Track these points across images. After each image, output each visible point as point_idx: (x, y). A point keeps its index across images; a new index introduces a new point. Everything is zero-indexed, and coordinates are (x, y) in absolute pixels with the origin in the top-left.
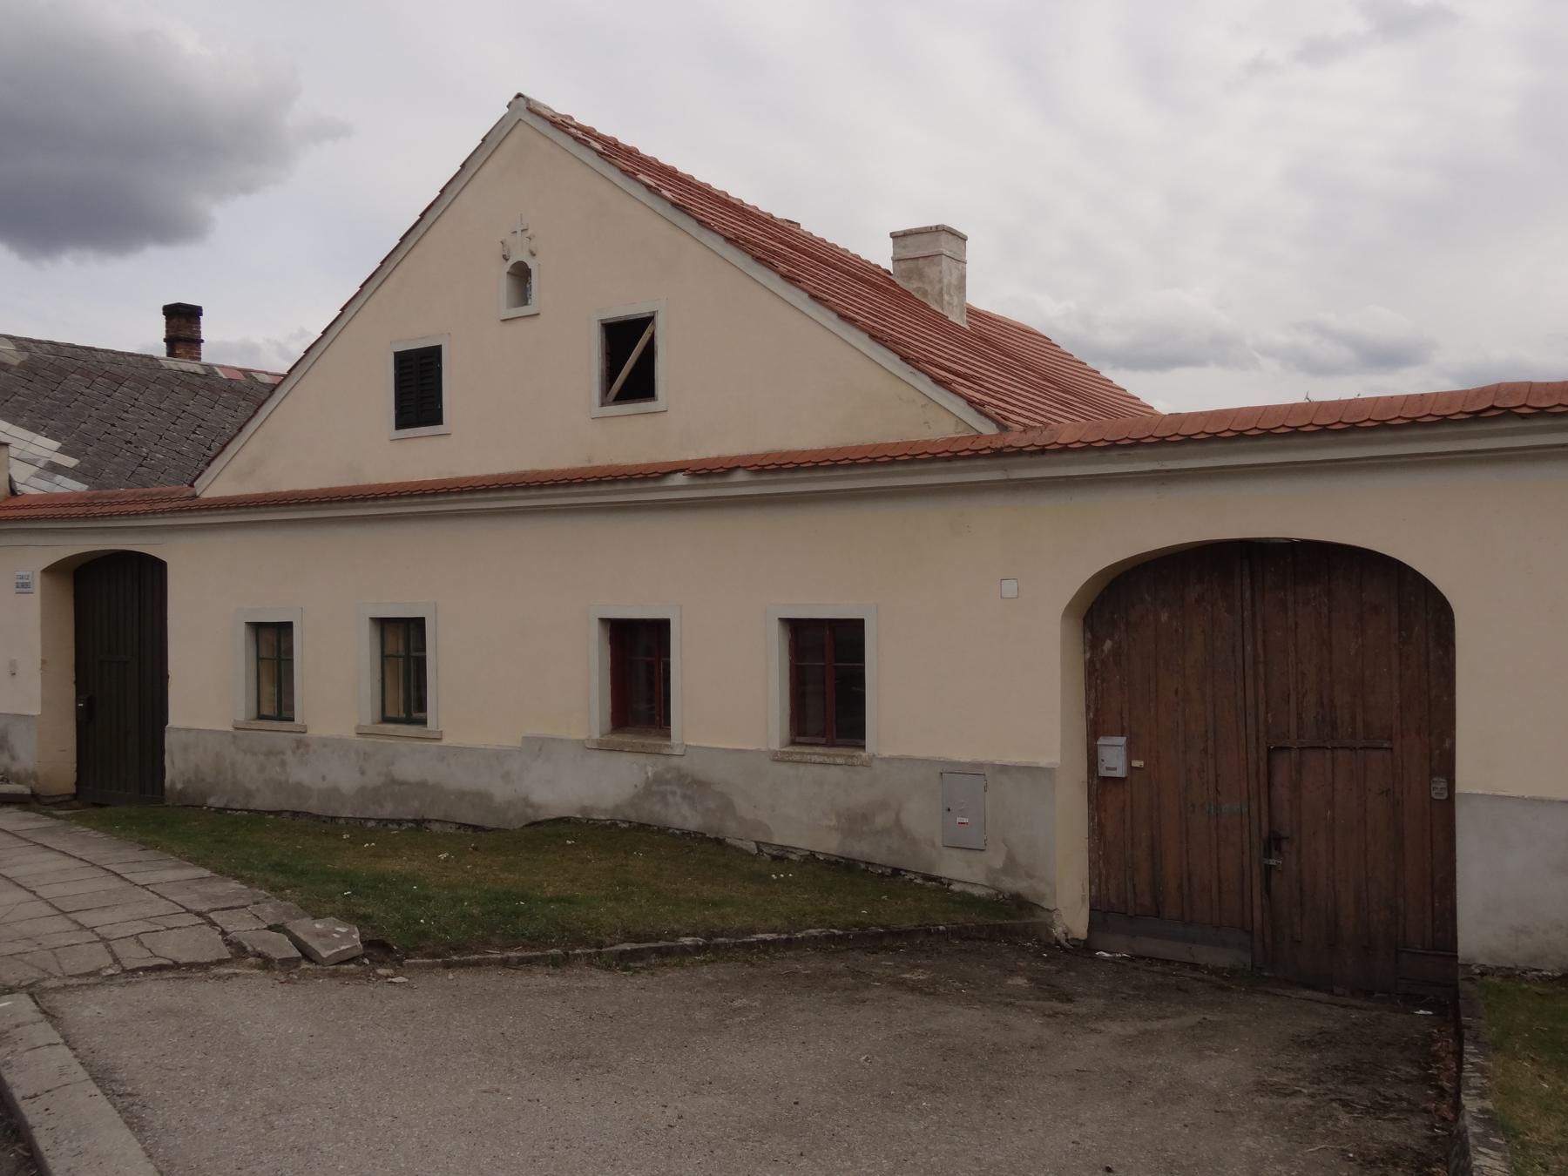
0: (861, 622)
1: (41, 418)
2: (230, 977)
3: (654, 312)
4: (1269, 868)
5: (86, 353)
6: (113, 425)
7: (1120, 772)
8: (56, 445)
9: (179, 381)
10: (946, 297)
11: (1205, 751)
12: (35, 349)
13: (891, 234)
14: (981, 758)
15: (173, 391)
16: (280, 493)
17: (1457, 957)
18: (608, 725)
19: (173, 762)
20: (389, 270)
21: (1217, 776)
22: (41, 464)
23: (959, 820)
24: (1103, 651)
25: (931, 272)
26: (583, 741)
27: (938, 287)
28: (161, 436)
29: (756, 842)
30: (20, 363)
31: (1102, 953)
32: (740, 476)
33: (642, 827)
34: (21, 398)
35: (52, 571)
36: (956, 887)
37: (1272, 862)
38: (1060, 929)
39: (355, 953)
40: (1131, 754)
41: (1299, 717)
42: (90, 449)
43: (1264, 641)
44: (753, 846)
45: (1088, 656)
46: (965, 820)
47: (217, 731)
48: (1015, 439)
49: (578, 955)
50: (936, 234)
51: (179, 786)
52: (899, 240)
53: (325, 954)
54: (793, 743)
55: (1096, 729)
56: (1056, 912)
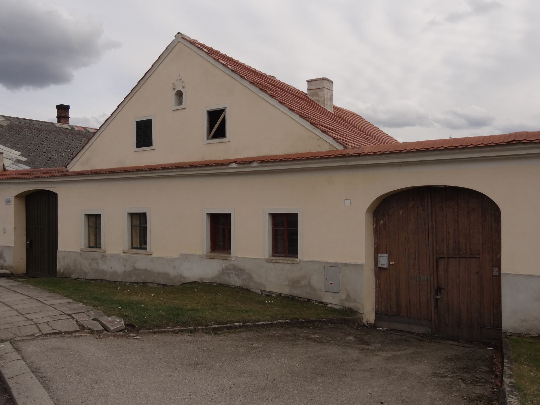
0: (297, 214)
1: (14, 144)
2: (79, 336)
3: (225, 108)
4: (437, 299)
5: (30, 122)
6: (39, 146)
7: (386, 266)
8: (19, 153)
9: (62, 131)
10: (326, 102)
11: (415, 259)
12: (12, 120)
13: (307, 80)
14: (338, 261)
15: (60, 135)
16: (97, 170)
17: (502, 330)
18: (209, 250)
19: (59, 263)
20: (134, 93)
21: (419, 267)
22: (14, 160)
23: (330, 282)
24: (380, 224)
25: (321, 94)
26: (201, 255)
27: (323, 99)
28: (55, 150)
29: (261, 290)
30: (7, 125)
31: (379, 328)
32: (255, 164)
33: (221, 285)
34: (7, 137)
35: (18, 197)
36: (329, 306)
37: (438, 297)
38: (365, 320)
39: (122, 328)
40: (389, 260)
41: (448, 247)
42: (31, 155)
43: (435, 221)
44: (259, 291)
45: (375, 226)
46: (332, 283)
47: (75, 252)
48: (350, 151)
49: (199, 329)
50: (323, 80)
51: (62, 271)
52: (309, 83)
53: (112, 328)
54: (273, 256)
55: (377, 251)
56: (364, 314)
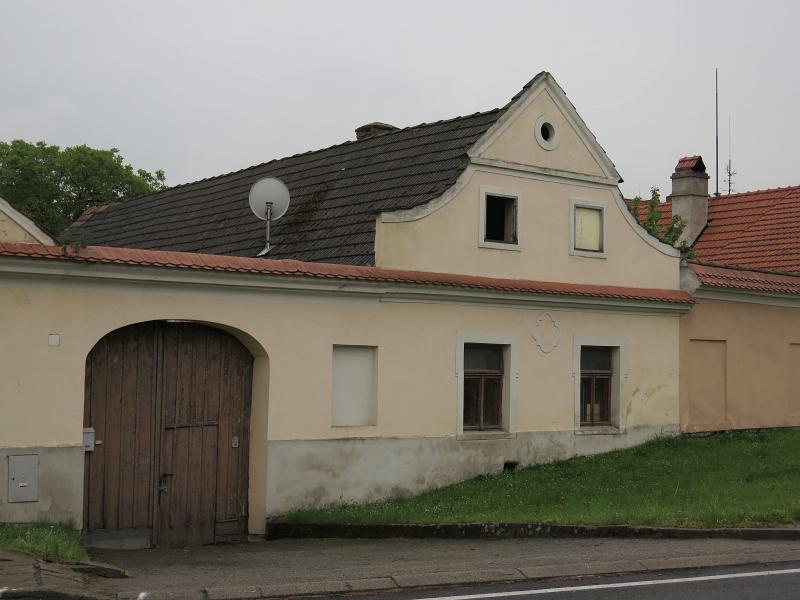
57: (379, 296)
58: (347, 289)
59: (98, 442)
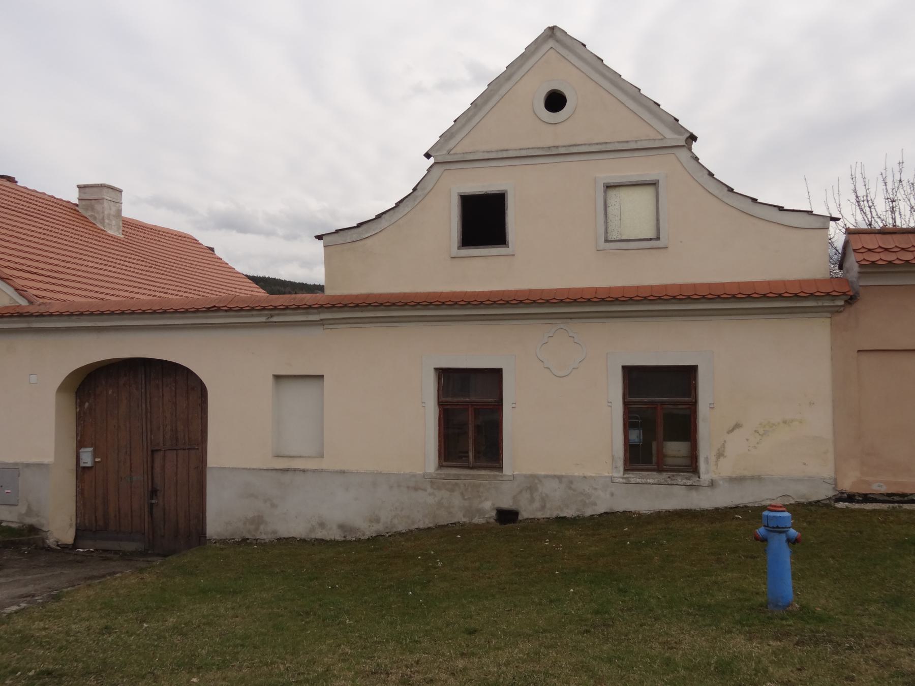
4: (152, 504)
7: (89, 465)
10: (107, 221)
11: (126, 452)
14: (18, 461)
17: (206, 537)
21: (131, 464)
23: (6, 491)
24: (84, 408)
25: (98, 207)
31: (79, 549)
36: (4, 524)
37: (153, 501)
38: (52, 540)
40: (95, 455)
41: (164, 436)
43: (150, 402)
45: (78, 410)
46: (9, 491)
48: (33, 309)
50: (102, 188)
52: (82, 189)
55: (80, 444)
56: (50, 532)
57: (322, 323)
58: (275, 319)
59: (98, 460)
